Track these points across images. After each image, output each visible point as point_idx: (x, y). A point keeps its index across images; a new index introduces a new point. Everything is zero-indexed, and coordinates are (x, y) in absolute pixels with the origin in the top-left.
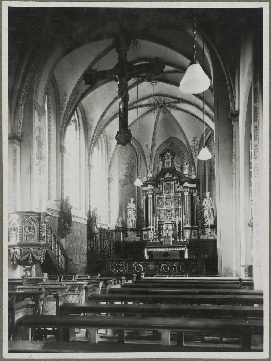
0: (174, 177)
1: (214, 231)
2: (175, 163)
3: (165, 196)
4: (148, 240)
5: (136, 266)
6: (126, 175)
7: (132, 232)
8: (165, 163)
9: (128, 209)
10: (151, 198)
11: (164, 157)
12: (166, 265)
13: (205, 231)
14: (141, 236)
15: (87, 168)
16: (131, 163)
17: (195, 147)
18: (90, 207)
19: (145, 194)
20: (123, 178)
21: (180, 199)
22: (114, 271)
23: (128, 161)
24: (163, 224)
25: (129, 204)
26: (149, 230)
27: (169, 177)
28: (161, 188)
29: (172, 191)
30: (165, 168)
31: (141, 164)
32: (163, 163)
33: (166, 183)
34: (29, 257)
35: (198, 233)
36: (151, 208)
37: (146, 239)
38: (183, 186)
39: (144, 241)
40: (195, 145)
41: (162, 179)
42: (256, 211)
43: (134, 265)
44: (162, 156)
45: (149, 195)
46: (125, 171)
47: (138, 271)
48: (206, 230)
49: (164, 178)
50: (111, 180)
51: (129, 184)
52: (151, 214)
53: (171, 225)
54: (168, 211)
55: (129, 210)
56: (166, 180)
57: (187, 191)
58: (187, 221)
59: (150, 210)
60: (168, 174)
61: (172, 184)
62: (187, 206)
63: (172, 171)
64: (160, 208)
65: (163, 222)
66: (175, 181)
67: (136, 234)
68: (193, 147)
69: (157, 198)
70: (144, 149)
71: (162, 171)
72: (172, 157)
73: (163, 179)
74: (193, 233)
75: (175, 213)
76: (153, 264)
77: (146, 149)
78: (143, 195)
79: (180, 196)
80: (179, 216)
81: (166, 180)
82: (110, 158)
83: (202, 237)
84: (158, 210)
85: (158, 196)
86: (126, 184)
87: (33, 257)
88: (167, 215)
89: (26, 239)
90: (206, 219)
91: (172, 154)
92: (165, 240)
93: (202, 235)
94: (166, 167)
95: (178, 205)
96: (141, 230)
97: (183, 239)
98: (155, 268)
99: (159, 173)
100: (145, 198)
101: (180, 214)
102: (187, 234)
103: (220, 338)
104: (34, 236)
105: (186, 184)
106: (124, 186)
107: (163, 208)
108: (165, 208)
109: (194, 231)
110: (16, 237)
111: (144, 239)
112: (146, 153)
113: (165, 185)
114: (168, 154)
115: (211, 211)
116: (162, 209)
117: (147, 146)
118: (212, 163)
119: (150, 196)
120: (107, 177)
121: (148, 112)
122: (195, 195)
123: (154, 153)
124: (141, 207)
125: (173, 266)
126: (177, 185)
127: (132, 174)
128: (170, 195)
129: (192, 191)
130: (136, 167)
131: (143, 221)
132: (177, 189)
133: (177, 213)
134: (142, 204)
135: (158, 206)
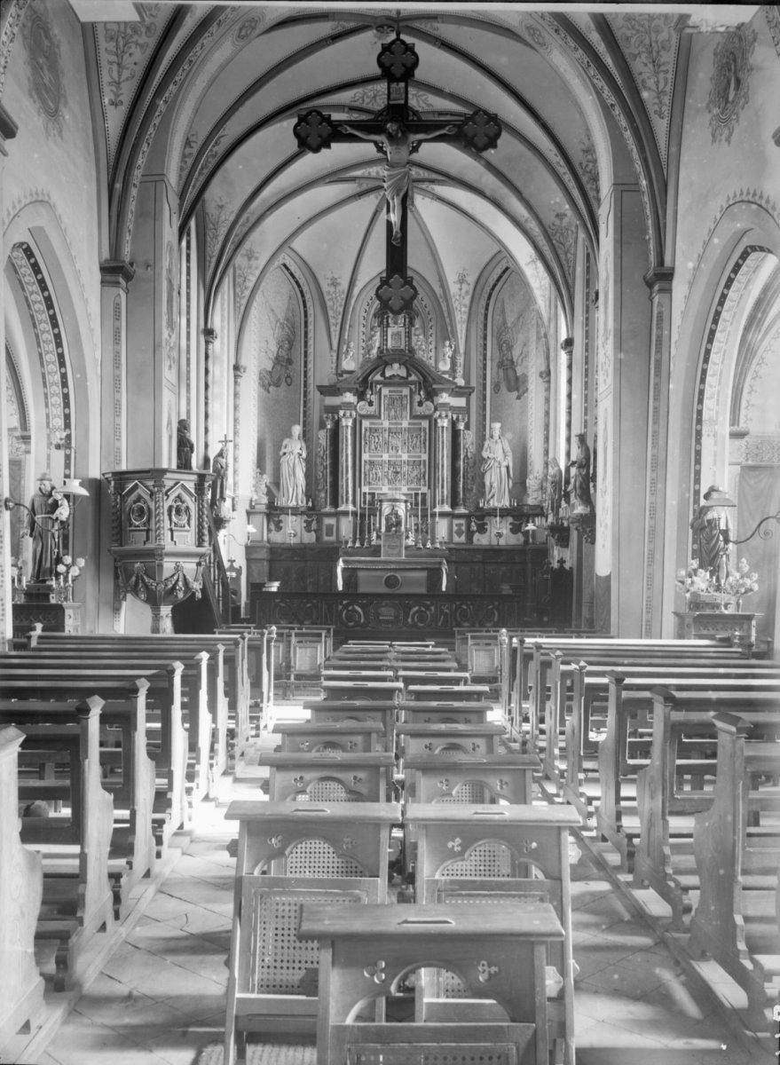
3: (386, 424)
4: (338, 541)
9: (285, 454)
12: (423, 609)
15: (202, 339)
18: (206, 446)
20: (269, 366)
24: (381, 501)
25: (286, 441)
26: (346, 513)
29: (404, 413)
30: (387, 350)
32: (384, 334)
34: (178, 580)
35: (469, 527)
36: (347, 461)
37: (333, 538)
38: (433, 402)
39: (327, 543)
43: (340, 607)
46: (274, 348)
47: (351, 624)
49: (385, 378)
52: (347, 467)
55: (287, 456)
56: (388, 382)
60: (396, 366)
63: (408, 358)
66: (413, 387)
71: (379, 357)
79: (425, 461)
85: (366, 424)
86: (277, 385)
89: (172, 539)
94: (389, 346)
97: (433, 543)
98: (396, 617)
101: (424, 476)
102: (442, 528)
105: (445, 398)
106: (271, 388)
108: (386, 457)
110: (145, 533)
111: (326, 538)
115: (504, 470)
117: (334, 283)
120: (233, 362)
122: (461, 426)
125: (442, 611)
126: (417, 398)
129: (455, 417)
132: (418, 408)
135: (367, 449)
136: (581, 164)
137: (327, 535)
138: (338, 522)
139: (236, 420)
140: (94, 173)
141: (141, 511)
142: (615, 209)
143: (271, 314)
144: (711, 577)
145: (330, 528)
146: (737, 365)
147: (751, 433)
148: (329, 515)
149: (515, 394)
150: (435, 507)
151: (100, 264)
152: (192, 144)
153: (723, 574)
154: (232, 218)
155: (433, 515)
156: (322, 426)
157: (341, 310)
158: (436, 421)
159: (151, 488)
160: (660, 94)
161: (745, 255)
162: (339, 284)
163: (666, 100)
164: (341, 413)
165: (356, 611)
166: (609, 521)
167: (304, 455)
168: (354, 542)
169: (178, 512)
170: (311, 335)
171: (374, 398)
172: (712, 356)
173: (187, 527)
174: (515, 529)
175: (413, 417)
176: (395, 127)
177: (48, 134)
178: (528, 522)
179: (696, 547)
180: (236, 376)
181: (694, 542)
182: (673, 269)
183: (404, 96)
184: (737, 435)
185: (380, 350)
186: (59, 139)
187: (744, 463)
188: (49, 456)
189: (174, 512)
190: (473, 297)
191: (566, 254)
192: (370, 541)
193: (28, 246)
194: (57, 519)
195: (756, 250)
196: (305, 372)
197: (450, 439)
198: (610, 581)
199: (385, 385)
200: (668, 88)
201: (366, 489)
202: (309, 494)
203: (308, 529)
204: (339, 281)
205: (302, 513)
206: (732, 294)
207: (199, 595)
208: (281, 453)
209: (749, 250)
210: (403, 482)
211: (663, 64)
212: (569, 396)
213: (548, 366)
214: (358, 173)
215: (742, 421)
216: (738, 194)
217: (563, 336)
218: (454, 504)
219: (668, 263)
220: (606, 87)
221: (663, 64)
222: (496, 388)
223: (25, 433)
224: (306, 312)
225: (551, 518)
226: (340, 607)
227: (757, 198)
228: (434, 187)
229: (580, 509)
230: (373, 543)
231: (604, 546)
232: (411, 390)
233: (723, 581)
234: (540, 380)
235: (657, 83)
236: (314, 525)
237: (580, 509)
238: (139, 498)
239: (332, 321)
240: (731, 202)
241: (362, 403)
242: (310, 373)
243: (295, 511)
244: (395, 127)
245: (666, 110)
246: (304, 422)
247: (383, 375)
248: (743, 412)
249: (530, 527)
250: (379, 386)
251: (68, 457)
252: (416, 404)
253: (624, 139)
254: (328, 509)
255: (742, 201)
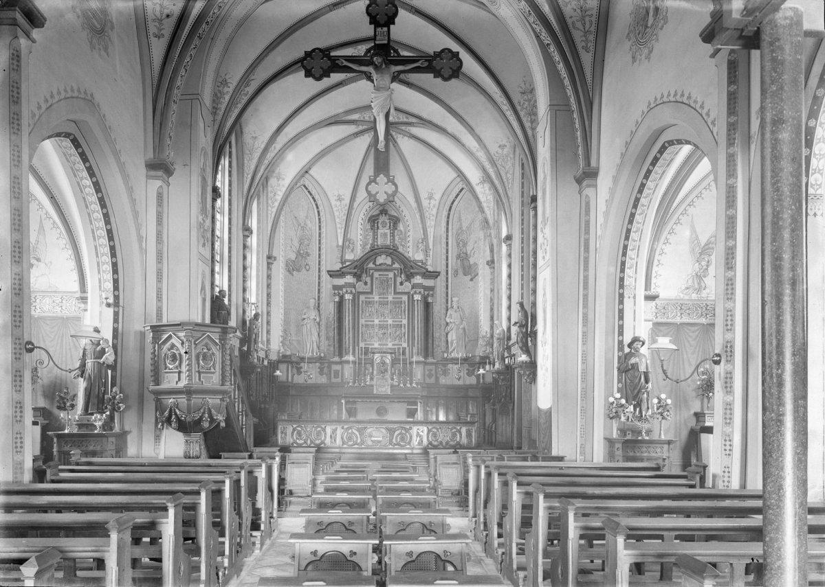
3: (376, 298)
12: (403, 432)
19: (336, 291)
26: (348, 362)
30: (377, 246)
34: (204, 413)
36: (349, 320)
37: (339, 380)
38: (410, 282)
41: (371, 265)
42: (727, 356)
49: (375, 265)
53: (389, 356)
69: (361, 302)
72: (392, 224)
74: (427, 373)
85: (362, 298)
87: (211, 416)
89: (200, 379)
94: (379, 243)
97: (411, 384)
103: (808, 552)
104: (213, 373)
105: (418, 280)
110: (177, 375)
112: (337, 210)
113: (377, 278)
121: (356, 135)
126: (399, 280)
128: (385, 298)
130: (318, 238)
132: (400, 287)
136: (519, 103)
138: (342, 369)
140: (141, 90)
141: (174, 358)
142: (551, 124)
143: (294, 221)
144: (635, 409)
145: (336, 373)
146: (650, 243)
147: (661, 296)
148: (336, 363)
149: (469, 277)
150: (412, 357)
151: (145, 162)
152: (229, 85)
153: (644, 407)
154: (263, 146)
155: (411, 363)
159: (183, 338)
160: (586, 33)
161: (663, 149)
162: (343, 199)
163: (592, 37)
166: (549, 364)
168: (354, 383)
169: (205, 358)
172: (632, 234)
173: (212, 370)
174: (470, 374)
175: (395, 293)
176: (380, 60)
177: (93, 47)
178: (479, 368)
179: (620, 385)
181: (619, 381)
182: (598, 169)
183: (387, 38)
184: (651, 298)
186: (103, 52)
187: (655, 320)
188: (101, 312)
189: (201, 358)
191: (506, 174)
192: (365, 382)
193: (75, 137)
194: (104, 363)
195: (673, 144)
198: (551, 412)
199: (376, 270)
200: (593, 29)
206: (650, 184)
207: (223, 424)
209: (667, 145)
211: (589, 10)
212: (510, 276)
213: (493, 257)
214: (355, 117)
215: (652, 289)
216: (666, 95)
217: (504, 233)
219: (593, 163)
220: (543, 30)
221: (589, 10)
222: (456, 273)
223: (83, 295)
225: (497, 366)
227: (685, 98)
228: (411, 128)
229: (524, 358)
230: (368, 383)
231: (544, 385)
232: (395, 274)
233: (644, 413)
234: (487, 267)
235: (584, 25)
236: (326, 370)
237: (524, 358)
238: (173, 346)
240: (652, 106)
244: (380, 60)
245: (591, 45)
248: (653, 280)
249: (481, 371)
250: (371, 271)
251: (116, 314)
252: (398, 283)
253: (558, 71)
254: (337, 359)
255: (663, 103)
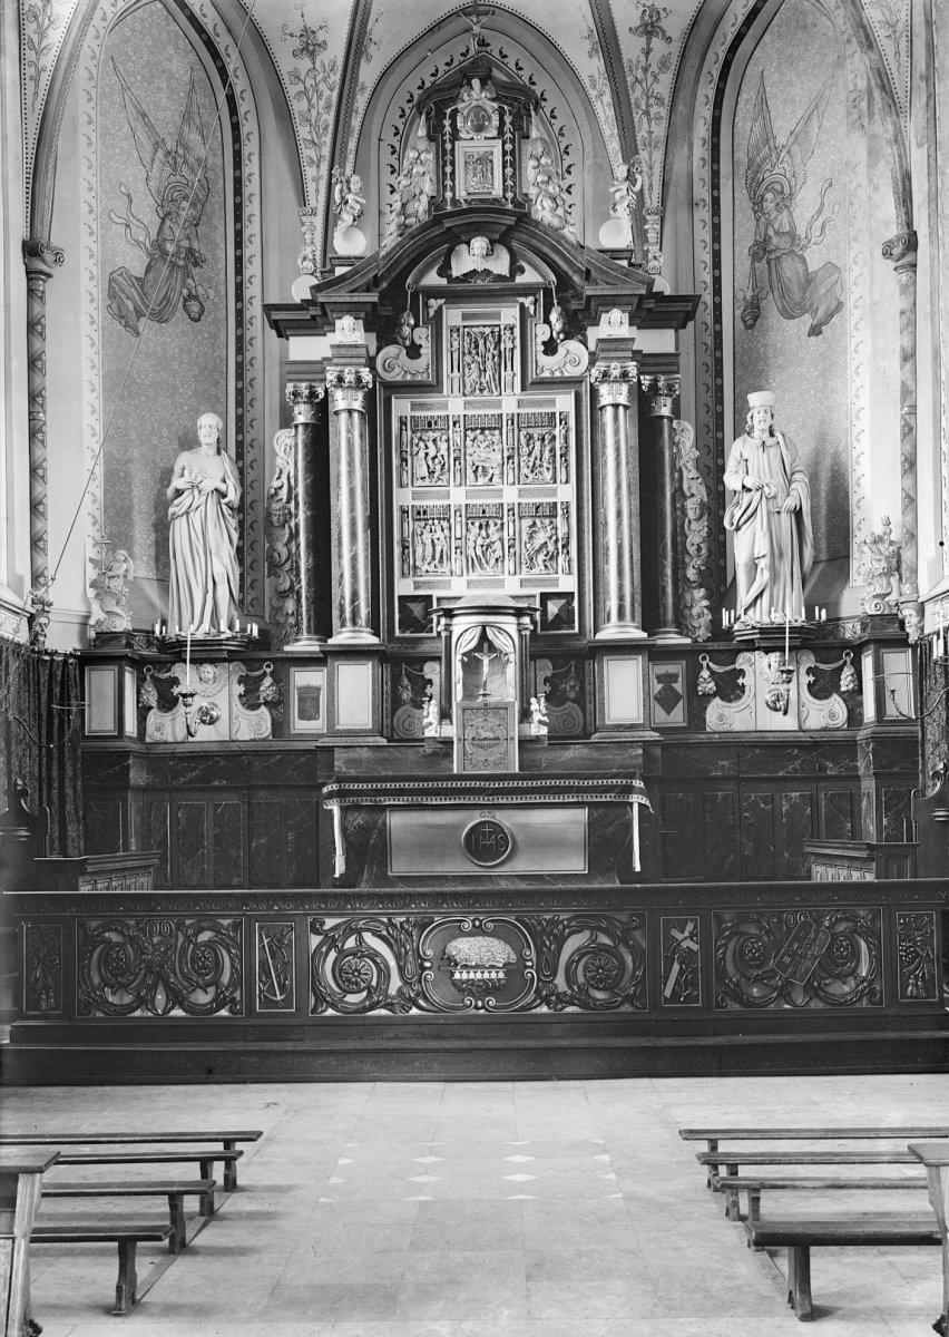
0: (522, 271)
1: (803, 670)
2: (532, 163)
5: (333, 955)
6: (159, 245)
7: (209, 670)
8: (453, 163)
9: (179, 493)
10: (356, 415)
11: (447, 122)
12: (604, 940)
13: (741, 673)
14: (277, 705)
16: (191, 160)
17: (650, 79)
21: (566, 438)
22: (128, 999)
23: (170, 145)
24: (449, 614)
25: (184, 459)
27: (487, 272)
28: (426, 351)
29: (506, 375)
30: (455, 202)
31: (266, 169)
32: (444, 159)
33: (465, 317)
36: (352, 492)
37: (316, 726)
39: (302, 737)
40: (654, 68)
43: (315, 940)
44: (436, 105)
45: (339, 394)
48: (742, 661)
49: (450, 279)
50: (49, 257)
51: (180, 314)
53: (510, 624)
54: (482, 518)
55: (185, 500)
56: (464, 291)
57: (625, 375)
58: (621, 598)
59: (352, 509)
60: (479, 244)
61: (503, 322)
62: (619, 487)
63: (508, 223)
64: (415, 496)
65: (439, 599)
66: (528, 301)
67: (241, 689)
68: (640, 74)
70: (286, 63)
72: (508, 119)
73: (444, 281)
75: (531, 537)
76: (492, 934)
77: (304, 64)
78: (296, 394)
79: (567, 506)
80: (554, 557)
81: (464, 291)
82: (36, 80)
83: (723, 717)
84: (404, 512)
85: (401, 407)
86: (160, 317)
88: (471, 552)
90: (752, 581)
91: (511, 101)
92: (470, 734)
93: (717, 700)
95: (548, 476)
96: (274, 660)
99: (413, 236)
100: (301, 419)
107: (438, 496)
108: (458, 497)
109: (662, 669)
111: (300, 726)
114: (476, 96)
115: (786, 522)
116: (430, 503)
118: (769, 196)
119: (345, 401)
120: (19, 232)
123: (361, 102)
124: (276, 484)
127: (196, 246)
129: (646, 380)
131: (293, 591)
132: (544, 360)
133: (541, 538)
134: (279, 462)
137: (303, 716)
139: (34, 397)
145: (309, 696)
149: (807, 321)
156: (286, 421)
157: (330, 118)
158: (594, 393)
162: (323, 45)
164: (331, 376)
165: (373, 955)
167: (233, 496)
170: (251, 187)
171: (422, 336)
180: (32, 275)
185: (435, 203)
190: (678, 76)
196: (239, 287)
197: (635, 441)
201: (404, 587)
202: (246, 602)
203: (250, 700)
204: (321, 36)
205: (232, 657)
208: (170, 492)
210: (509, 564)
213: (909, 224)
218: (651, 622)
224: (236, 127)
226: (315, 940)
232: (523, 308)
236: (267, 687)
239: (307, 153)
241: (391, 350)
242: (252, 270)
243: (207, 653)
246: (240, 445)
247: (444, 271)
254: (306, 644)
